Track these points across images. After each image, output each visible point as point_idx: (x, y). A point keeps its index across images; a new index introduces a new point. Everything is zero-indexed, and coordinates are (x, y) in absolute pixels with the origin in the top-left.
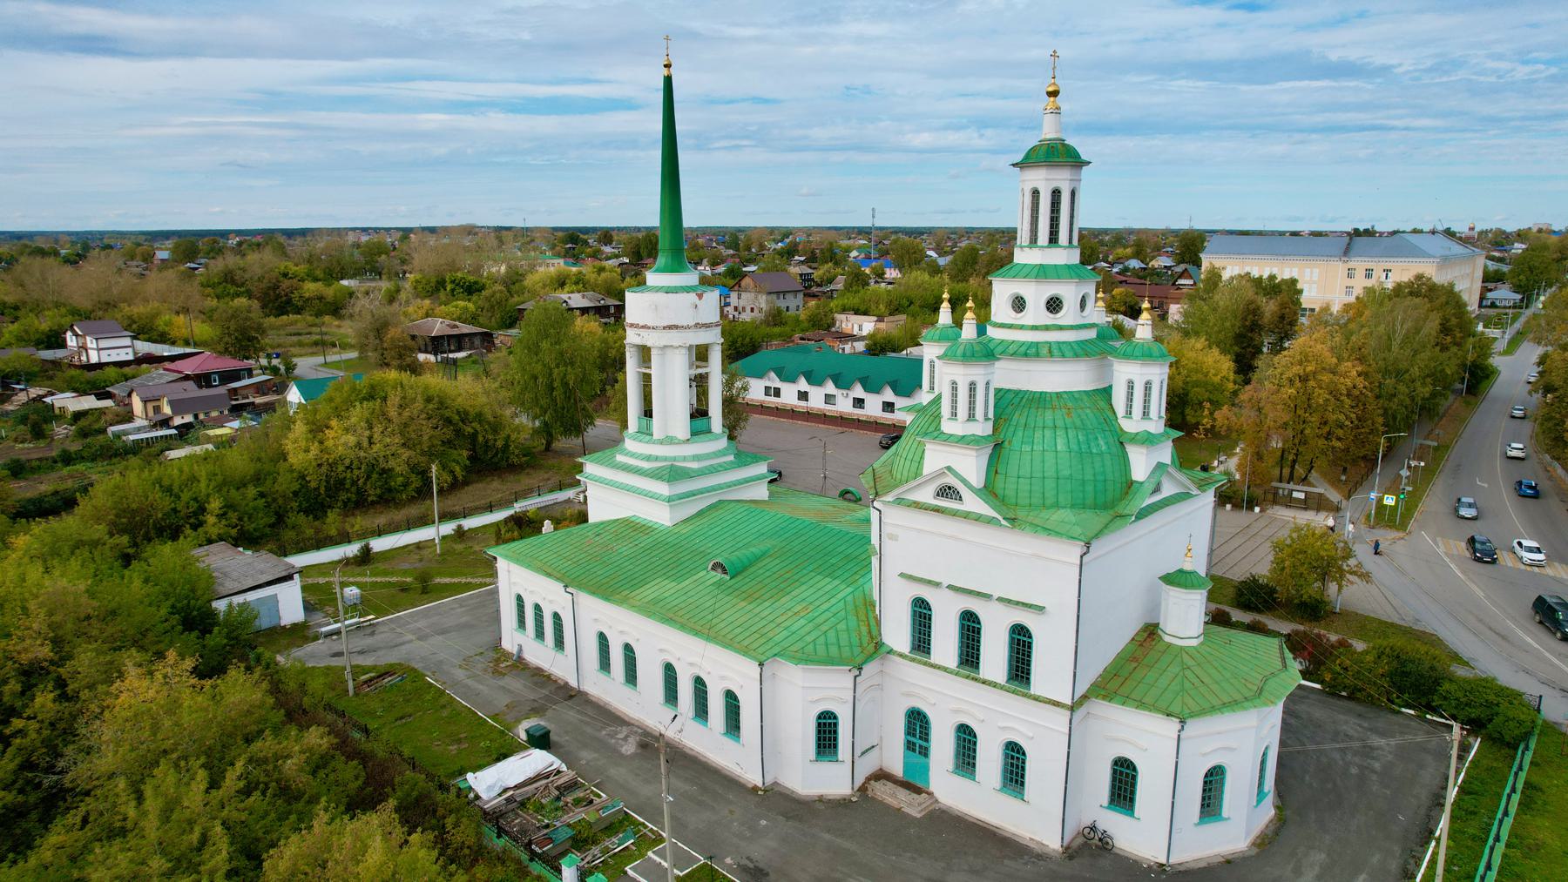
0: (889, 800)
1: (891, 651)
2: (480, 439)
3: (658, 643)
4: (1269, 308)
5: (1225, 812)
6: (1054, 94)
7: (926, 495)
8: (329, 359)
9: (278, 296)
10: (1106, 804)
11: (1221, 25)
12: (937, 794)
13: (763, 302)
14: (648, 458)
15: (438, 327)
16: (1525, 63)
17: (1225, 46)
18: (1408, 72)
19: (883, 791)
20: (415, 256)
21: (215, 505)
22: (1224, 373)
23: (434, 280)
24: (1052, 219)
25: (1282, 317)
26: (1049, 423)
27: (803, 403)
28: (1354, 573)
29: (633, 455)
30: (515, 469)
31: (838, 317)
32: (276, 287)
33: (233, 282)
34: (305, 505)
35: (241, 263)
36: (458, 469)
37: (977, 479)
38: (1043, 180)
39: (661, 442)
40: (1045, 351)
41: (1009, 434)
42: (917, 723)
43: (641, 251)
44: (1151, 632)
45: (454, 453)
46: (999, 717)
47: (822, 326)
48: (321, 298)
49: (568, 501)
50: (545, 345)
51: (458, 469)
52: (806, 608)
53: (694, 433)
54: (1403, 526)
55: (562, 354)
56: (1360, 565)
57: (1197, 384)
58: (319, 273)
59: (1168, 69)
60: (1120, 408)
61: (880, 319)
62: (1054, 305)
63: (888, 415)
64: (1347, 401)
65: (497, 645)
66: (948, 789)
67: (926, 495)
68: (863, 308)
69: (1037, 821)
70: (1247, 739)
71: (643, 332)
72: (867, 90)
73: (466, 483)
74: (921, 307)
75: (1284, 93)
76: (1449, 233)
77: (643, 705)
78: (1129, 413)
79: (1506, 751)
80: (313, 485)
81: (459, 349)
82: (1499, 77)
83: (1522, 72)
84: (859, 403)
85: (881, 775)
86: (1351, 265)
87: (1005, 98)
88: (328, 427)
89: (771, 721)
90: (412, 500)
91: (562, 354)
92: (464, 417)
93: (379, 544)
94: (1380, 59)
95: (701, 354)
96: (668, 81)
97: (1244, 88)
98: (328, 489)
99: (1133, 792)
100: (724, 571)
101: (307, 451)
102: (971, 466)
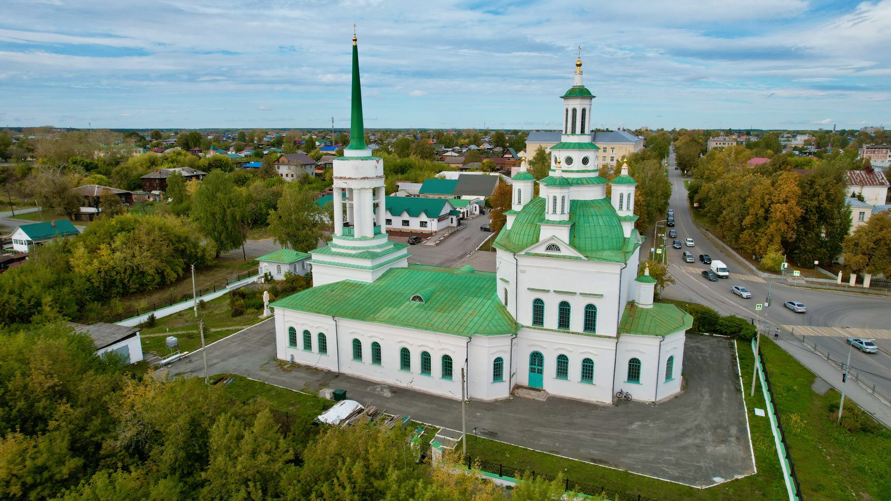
0: (527, 396)
1: (523, 326)
3: (393, 338)
5: (673, 377)
6: (580, 65)
7: (541, 250)
8: (16, 212)
10: (626, 379)
11: (481, 21)
12: (547, 390)
14: (354, 248)
16: (621, 49)
17: (484, 32)
19: (521, 393)
20: (39, 146)
21: (47, 299)
29: (340, 247)
34: (93, 297)
37: (566, 239)
38: (577, 104)
39: (360, 239)
42: (537, 359)
43: (339, 141)
44: (631, 305)
45: (176, 261)
46: (577, 347)
49: (254, 283)
50: (219, 195)
52: (474, 312)
53: (375, 234)
55: (230, 200)
59: (458, 43)
62: (585, 161)
63: (423, 229)
65: (274, 358)
66: (552, 385)
67: (541, 250)
69: (600, 392)
70: (676, 344)
71: (348, 181)
72: (293, 49)
75: (517, 58)
76: (629, 131)
77: (389, 373)
78: (621, 207)
79: (746, 343)
80: (96, 284)
83: (620, 54)
85: (518, 387)
87: (373, 56)
89: (473, 367)
90: (156, 290)
91: (230, 200)
92: (179, 240)
93: (159, 314)
94: (559, 43)
95: (375, 192)
96: (355, 48)
97: (497, 54)
98: (105, 286)
99: (639, 373)
100: (421, 300)
101: (90, 263)
102: (563, 234)
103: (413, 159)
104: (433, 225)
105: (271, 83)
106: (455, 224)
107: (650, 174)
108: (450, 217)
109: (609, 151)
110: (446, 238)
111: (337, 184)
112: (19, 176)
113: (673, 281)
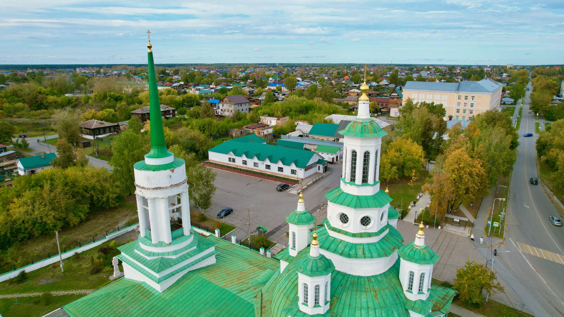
2: (95, 198)
4: (434, 118)
9: (37, 102)
13: (232, 108)
15: (95, 124)
18: (472, 8)
20: (96, 85)
22: (420, 154)
23: (102, 95)
24: (364, 169)
25: (441, 126)
26: (364, 305)
27: (244, 166)
28: (495, 287)
30: (112, 209)
31: (262, 117)
32: (36, 98)
33: (17, 96)
35: (21, 88)
36: (82, 215)
39: (156, 246)
40: (360, 252)
41: (340, 310)
47: (255, 121)
48: (56, 102)
50: (126, 152)
51: (82, 215)
53: (174, 238)
54: (501, 236)
56: (499, 284)
57: (409, 160)
58: (55, 91)
60: (405, 286)
61: (278, 119)
62: (365, 221)
64: (476, 178)
68: (271, 113)
73: (87, 220)
74: (295, 111)
78: (410, 288)
81: (105, 133)
82: (502, 11)
84: (268, 167)
86: (460, 94)
88: (12, 202)
93: (28, 269)
103: (317, 101)
104: (301, 174)
105: (267, 34)
106: (321, 171)
107: (495, 142)
108: (318, 165)
109: (470, 98)
110: (309, 186)
111: (138, 192)
112: (83, 103)
113: (501, 289)
